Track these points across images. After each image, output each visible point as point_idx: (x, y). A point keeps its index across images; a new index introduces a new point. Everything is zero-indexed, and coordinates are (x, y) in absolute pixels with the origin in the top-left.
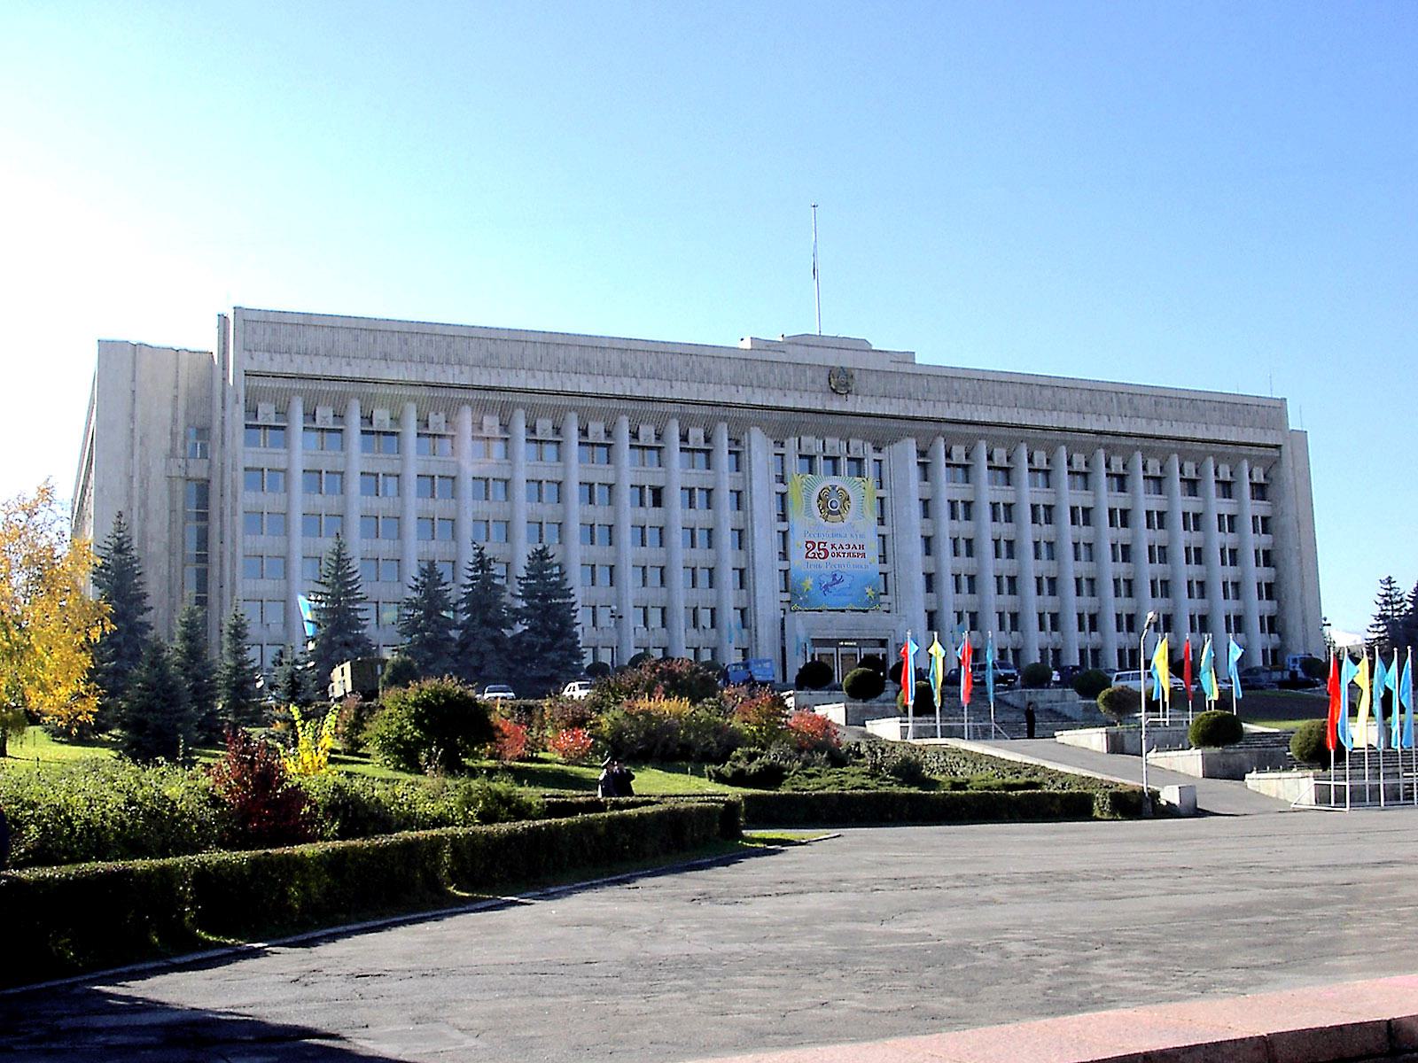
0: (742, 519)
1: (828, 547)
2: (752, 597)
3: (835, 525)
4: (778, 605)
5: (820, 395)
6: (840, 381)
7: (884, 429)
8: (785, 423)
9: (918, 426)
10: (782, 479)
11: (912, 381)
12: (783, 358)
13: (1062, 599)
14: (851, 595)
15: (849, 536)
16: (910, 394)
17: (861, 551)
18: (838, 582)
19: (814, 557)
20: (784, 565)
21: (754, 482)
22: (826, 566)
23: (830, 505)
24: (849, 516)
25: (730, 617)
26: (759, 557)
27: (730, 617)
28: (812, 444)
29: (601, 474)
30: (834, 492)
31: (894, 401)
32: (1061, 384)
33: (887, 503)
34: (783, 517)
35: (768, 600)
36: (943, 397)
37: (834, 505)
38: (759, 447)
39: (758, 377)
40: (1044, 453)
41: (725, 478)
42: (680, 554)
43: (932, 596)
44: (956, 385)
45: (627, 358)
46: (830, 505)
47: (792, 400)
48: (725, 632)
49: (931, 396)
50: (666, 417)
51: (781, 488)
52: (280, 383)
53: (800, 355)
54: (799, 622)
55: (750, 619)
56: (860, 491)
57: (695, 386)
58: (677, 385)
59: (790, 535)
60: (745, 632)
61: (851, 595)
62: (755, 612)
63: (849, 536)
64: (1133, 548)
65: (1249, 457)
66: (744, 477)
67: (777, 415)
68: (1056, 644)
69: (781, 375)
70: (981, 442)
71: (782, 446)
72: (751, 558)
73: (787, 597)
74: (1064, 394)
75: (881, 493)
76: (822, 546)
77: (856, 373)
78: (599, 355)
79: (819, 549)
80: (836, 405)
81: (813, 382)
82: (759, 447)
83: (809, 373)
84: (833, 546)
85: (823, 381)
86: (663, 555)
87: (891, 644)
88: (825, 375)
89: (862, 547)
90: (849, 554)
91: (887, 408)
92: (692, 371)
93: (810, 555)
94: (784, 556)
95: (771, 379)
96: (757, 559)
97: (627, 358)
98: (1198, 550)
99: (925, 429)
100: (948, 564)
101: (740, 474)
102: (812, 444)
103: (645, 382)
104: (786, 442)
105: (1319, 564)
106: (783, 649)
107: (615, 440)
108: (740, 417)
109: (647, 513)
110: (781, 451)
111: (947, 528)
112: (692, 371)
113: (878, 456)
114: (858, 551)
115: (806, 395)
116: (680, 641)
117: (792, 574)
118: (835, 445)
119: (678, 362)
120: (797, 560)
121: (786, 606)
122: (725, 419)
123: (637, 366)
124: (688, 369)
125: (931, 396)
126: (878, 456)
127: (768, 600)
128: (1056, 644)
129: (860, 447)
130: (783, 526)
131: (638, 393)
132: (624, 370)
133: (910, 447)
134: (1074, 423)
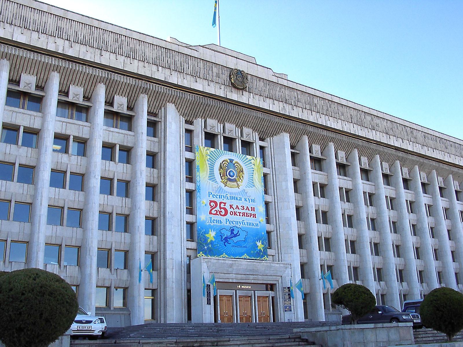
0: (156, 176)
1: (227, 207)
2: (162, 243)
3: (231, 189)
4: (185, 253)
5: (223, 87)
6: (239, 80)
7: (270, 123)
8: (196, 105)
9: (292, 124)
10: (190, 149)
11: (287, 92)
12: (195, 54)
13: (384, 258)
14: (245, 247)
15: (243, 200)
16: (286, 100)
17: (253, 212)
18: (236, 236)
19: (216, 214)
20: (190, 218)
21: (168, 146)
22: (226, 221)
23: (230, 174)
24: (243, 184)
25: (140, 258)
26: (169, 207)
27: (140, 258)
28: (214, 125)
29: (74, 128)
30: (232, 164)
31: (276, 102)
32: (344, 103)
33: (270, 178)
34: (190, 178)
35: (176, 245)
36: (308, 107)
37: (231, 174)
38: (173, 122)
39: (175, 64)
40: (366, 158)
41: (144, 143)
42: (97, 201)
43: (304, 251)
44: (315, 101)
45: (63, 24)
46: (230, 174)
47: (201, 86)
48: (136, 274)
49: (300, 104)
50: (94, 82)
51: (189, 155)
52: (131, 81)
53: (208, 55)
54: (204, 266)
55: (159, 262)
56: (251, 166)
57: (121, 59)
58: (106, 54)
59: (197, 195)
60: (155, 273)
61: (245, 247)
62: (165, 255)
63: (243, 200)
64: (418, 227)
65: (309, 134)
66: (160, 142)
67: (189, 96)
68: (383, 290)
69: (194, 66)
70: (142, 95)
71: (191, 124)
72: (163, 210)
73: (193, 245)
74: (378, 121)
75: (266, 170)
76: (222, 205)
77: (249, 77)
78: (37, 16)
79: (221, 208)
80: (234, 96)
81: (218, 76)
82: (173, 122)
83: (215, 70)
84: (231, 206)
85: (225, 76)
86: (82, 198)
87: (279, 288)
88: (227, 73)
89: (253, 209)
90: (244, 214)
91: (180, 80)
92: (120, 47)
93: (213, 212)
94: (190, 211)
95: (186, 66)
96: (168, 210)
97: (63, 24)
98: (327, 240)
99: (298, 127)
100: (316, 229)
101: (156, 139)
102: (214, 125)
103: (77, 46)
104: (195, 121)
105: (151, 312)
106: (189, 291)
107: (46, 93)
108: (162, 92)
109: (70, 160)
110: (190, 127)
111: (313, 202)
112: (120, 47)
113: (262, 144)
114: (240, 211)
115: (212, 84)
116: (90, 279)
117: (196, 228)
118: (232, 130)
119: (109, 38)
120: (203, 215)
121: (191, 253)
122: (145, 91)
123: (71, 33)
124: (117, 45)
125: (300, 104)
126: (262, 144)
127: (176, 245)
128: (383, 290)
129: (250, 134)
130: (190, 186)
131: (70, 52)
132: (59, 33)
133: (286, 138)
134: (384, 140)
